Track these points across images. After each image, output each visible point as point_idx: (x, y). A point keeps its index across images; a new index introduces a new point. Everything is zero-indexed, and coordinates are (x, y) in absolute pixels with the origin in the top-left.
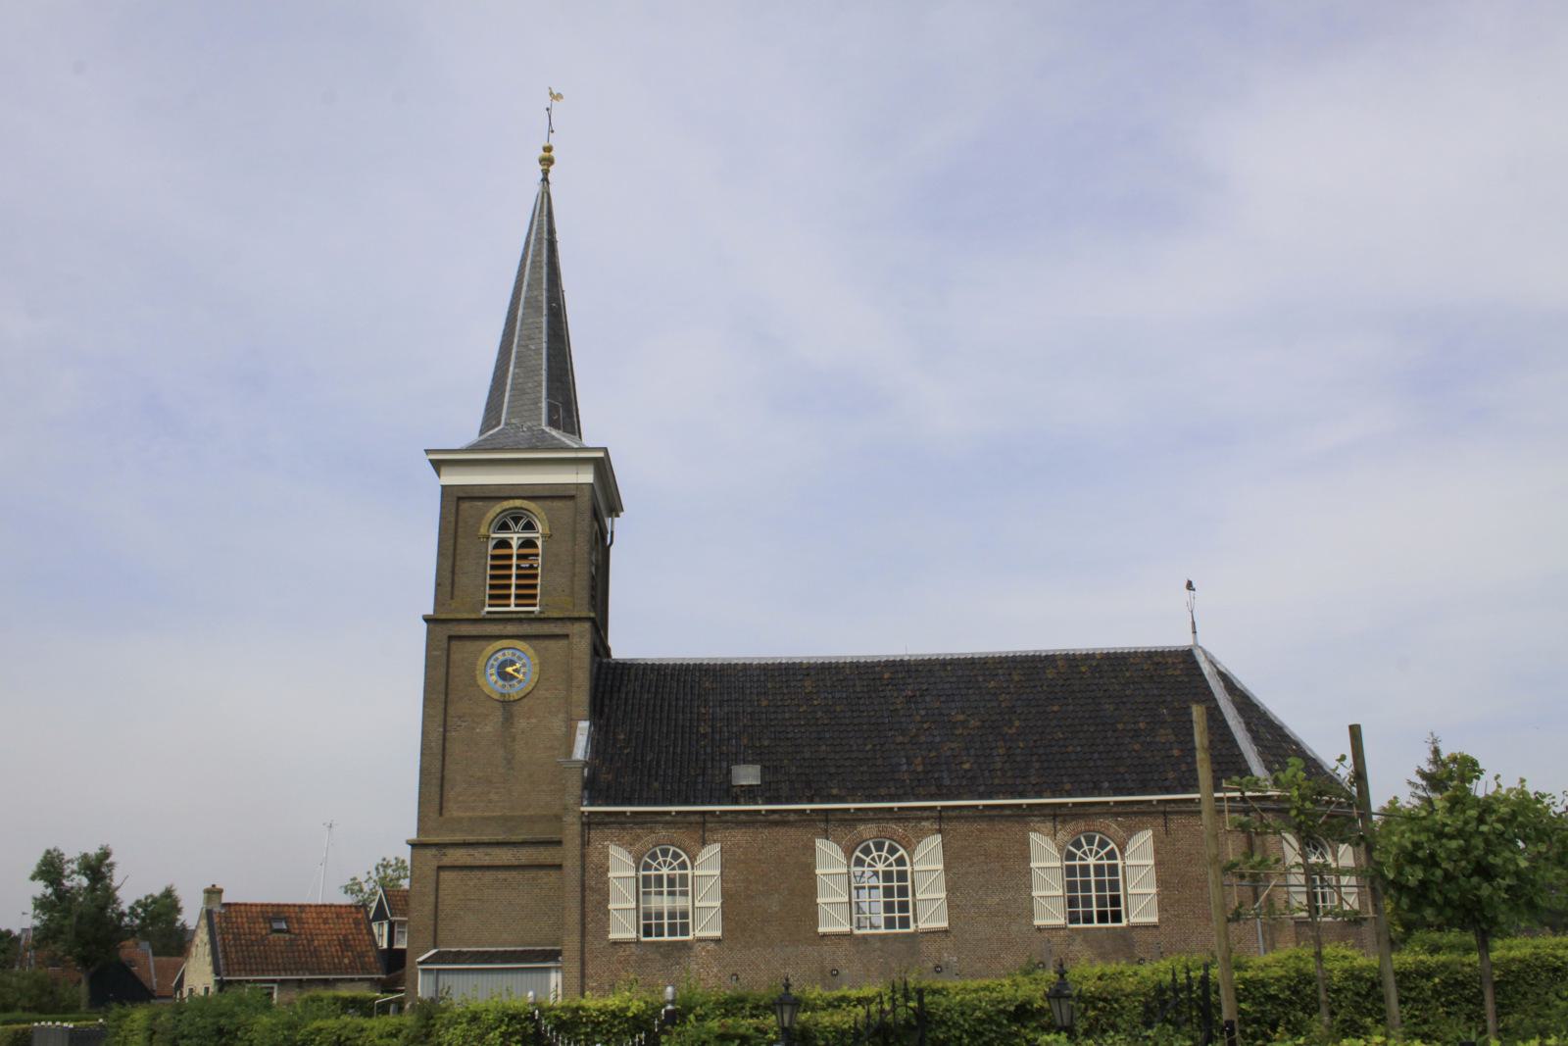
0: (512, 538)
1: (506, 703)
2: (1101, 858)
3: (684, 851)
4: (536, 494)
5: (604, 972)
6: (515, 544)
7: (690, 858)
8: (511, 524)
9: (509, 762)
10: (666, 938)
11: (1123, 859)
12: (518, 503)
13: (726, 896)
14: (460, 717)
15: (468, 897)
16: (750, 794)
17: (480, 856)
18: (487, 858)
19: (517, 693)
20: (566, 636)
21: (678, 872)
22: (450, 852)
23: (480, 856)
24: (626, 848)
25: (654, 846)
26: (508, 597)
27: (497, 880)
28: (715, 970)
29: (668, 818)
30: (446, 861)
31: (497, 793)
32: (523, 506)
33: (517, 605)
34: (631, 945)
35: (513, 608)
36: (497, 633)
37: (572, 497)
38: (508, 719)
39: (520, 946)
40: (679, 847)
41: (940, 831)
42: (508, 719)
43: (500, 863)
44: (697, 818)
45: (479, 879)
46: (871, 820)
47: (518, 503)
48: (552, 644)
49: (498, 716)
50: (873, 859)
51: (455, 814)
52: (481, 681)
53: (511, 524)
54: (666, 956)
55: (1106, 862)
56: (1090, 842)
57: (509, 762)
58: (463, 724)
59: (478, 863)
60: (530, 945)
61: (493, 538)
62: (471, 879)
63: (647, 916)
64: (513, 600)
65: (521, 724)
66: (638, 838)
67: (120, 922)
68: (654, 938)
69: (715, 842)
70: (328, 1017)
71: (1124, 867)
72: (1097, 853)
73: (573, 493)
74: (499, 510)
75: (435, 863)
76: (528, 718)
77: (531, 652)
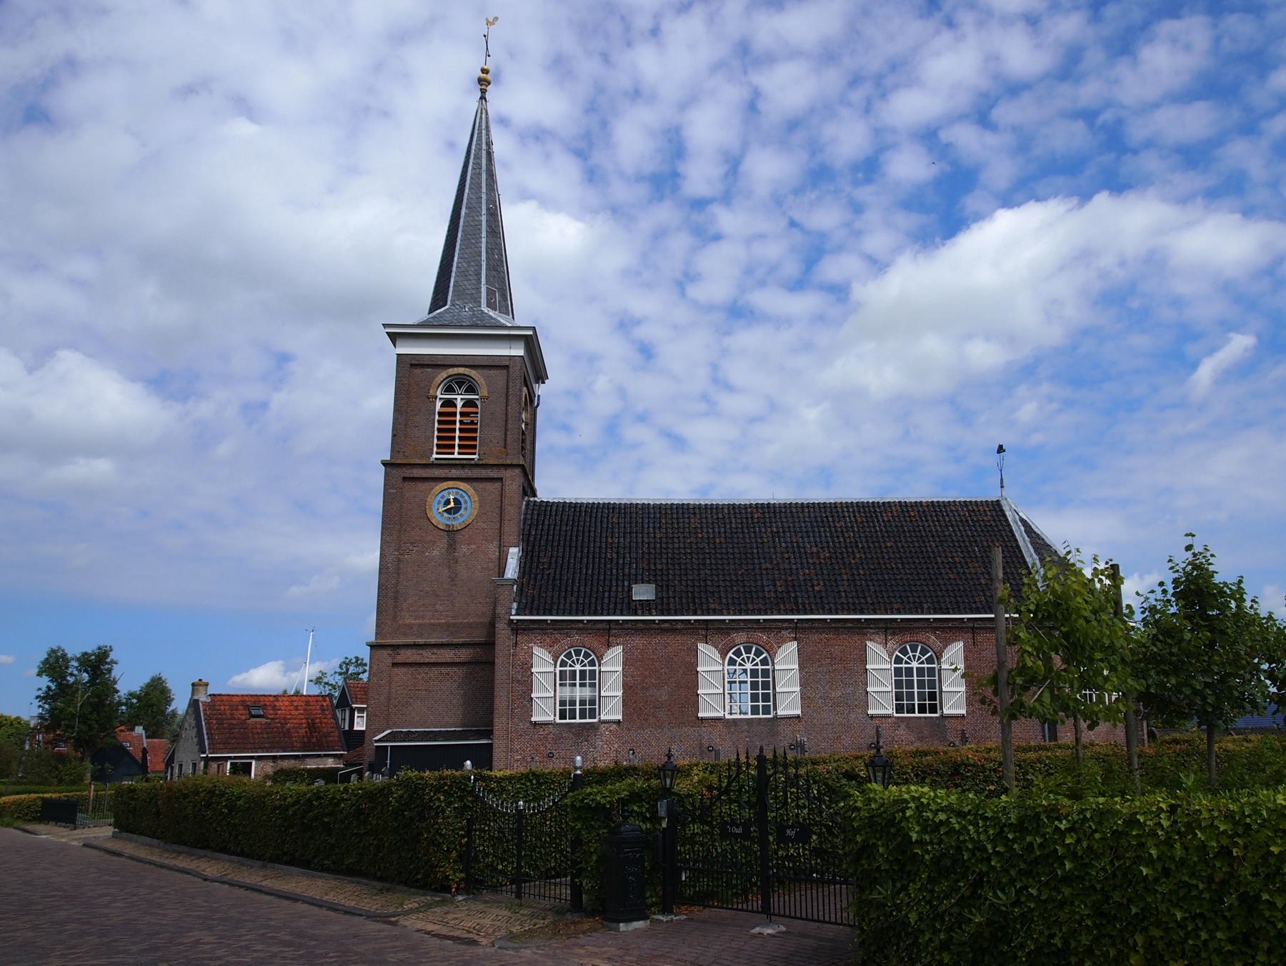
0: (456, 399)
1: (451, 532)
5: (527, 747)
6: (459, 404)
8: (456, 387)
10: (578, 720)
12: (461, 370)
13: (626, 687)
14: (412, 543)
16: (645, 607)
17: (428, 656)
18: (433, 656)
19: (460, 524)
20: (501, 479)
21: (588, 668)
22: (402, 652)
23: (428, 656)
27: (441, 674)
28: (616, 746)
29: (581, 625)
30: (399, 659)
31: (441, 604)
32: (466, 373)
33: (459, 454)
35: (456, 456)
36: (444, 476)
37: (507, 367)
38: (452, 546)
42: (452, 546)
43: (443, 661)
44: (603, 626)
45: (427, 673)
46: (742, 629)
47: (461, 370)
48: (489, 486)
49: (443, 542)
50: (582, 661)
51: (408, 621)
53: (456, 387)
54: (578, 735)
55: (588, 668)
58: (415, 549)
59: (427, 660)
62: (419, 674)
63: (563, 703)
65: (463, 549)
66: (556, 641)
68: (568, 721)
73: (507, 363)
74: (445, 376)
75: (389, 661)
76: (469, 544)
77: (471, 492)
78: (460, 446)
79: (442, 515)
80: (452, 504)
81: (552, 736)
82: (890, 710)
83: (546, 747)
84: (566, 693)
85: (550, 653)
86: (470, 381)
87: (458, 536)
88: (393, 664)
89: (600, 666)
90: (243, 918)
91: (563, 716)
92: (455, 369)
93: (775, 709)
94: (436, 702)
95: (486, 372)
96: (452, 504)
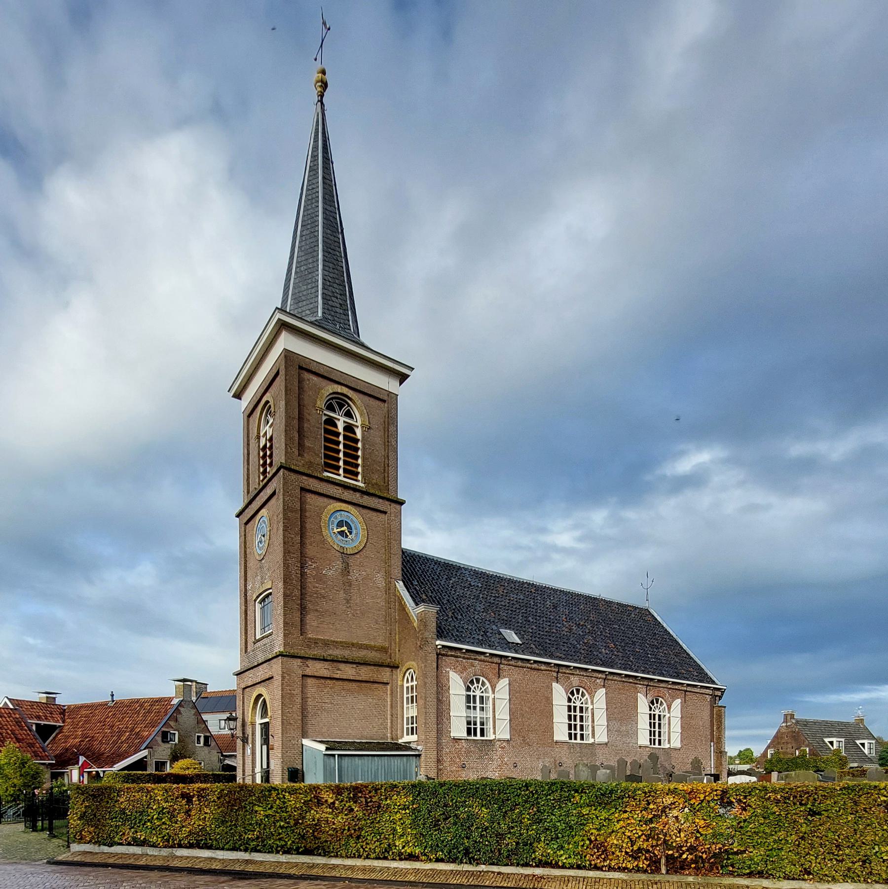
0: (339, 420)
1: (344, 555)
2: (482, 692)
3: (489, 681)
4: (358, 388)
7: (491, 686)
9: (348, 601)
11: (494, 692)
12: (345, 390)
15: (324, 701)
18: (338, 672)
24: (459, 675)
25: (474, 676)
26: (338, 468)
29: (482, 657)
30: (308, 672)
32: (349, 395)
33: (344, 477)
34: (463, 741)
35: (341, 478)
39: (358, 739)
40: (486, 678)
41: (604, 686)
47: (345, 390)
49: (338, 564)
52: (325, 532)
56: (578, 693)
57: (348, 601)
58: (314, 565)
60: (367, 739)
61: (325, 414)
63: (469, 723)
64: (341, 471)
67: (594, 779)
69: (505, 677)
70: (148, 782)
71: (494, 699)
72: (481, 689)
73: (385, 398)
75: (300, 672)
78: (345, 471)
79: (336, 537)
80: (344, 528)
81: (464, 749)
82: (464, 734)
83: (460, 759)
84: (478, 709)
85: (461, 678)
86: (349, 405)
87: (351, 561)
88: (303, 676)
89: (494, 692)
90: (126, 772)
91: (469, 733)
92: (340, 387)
93: (593, 736)
94: (340, 715)
95: (366, 398)
96: (344, 528)
